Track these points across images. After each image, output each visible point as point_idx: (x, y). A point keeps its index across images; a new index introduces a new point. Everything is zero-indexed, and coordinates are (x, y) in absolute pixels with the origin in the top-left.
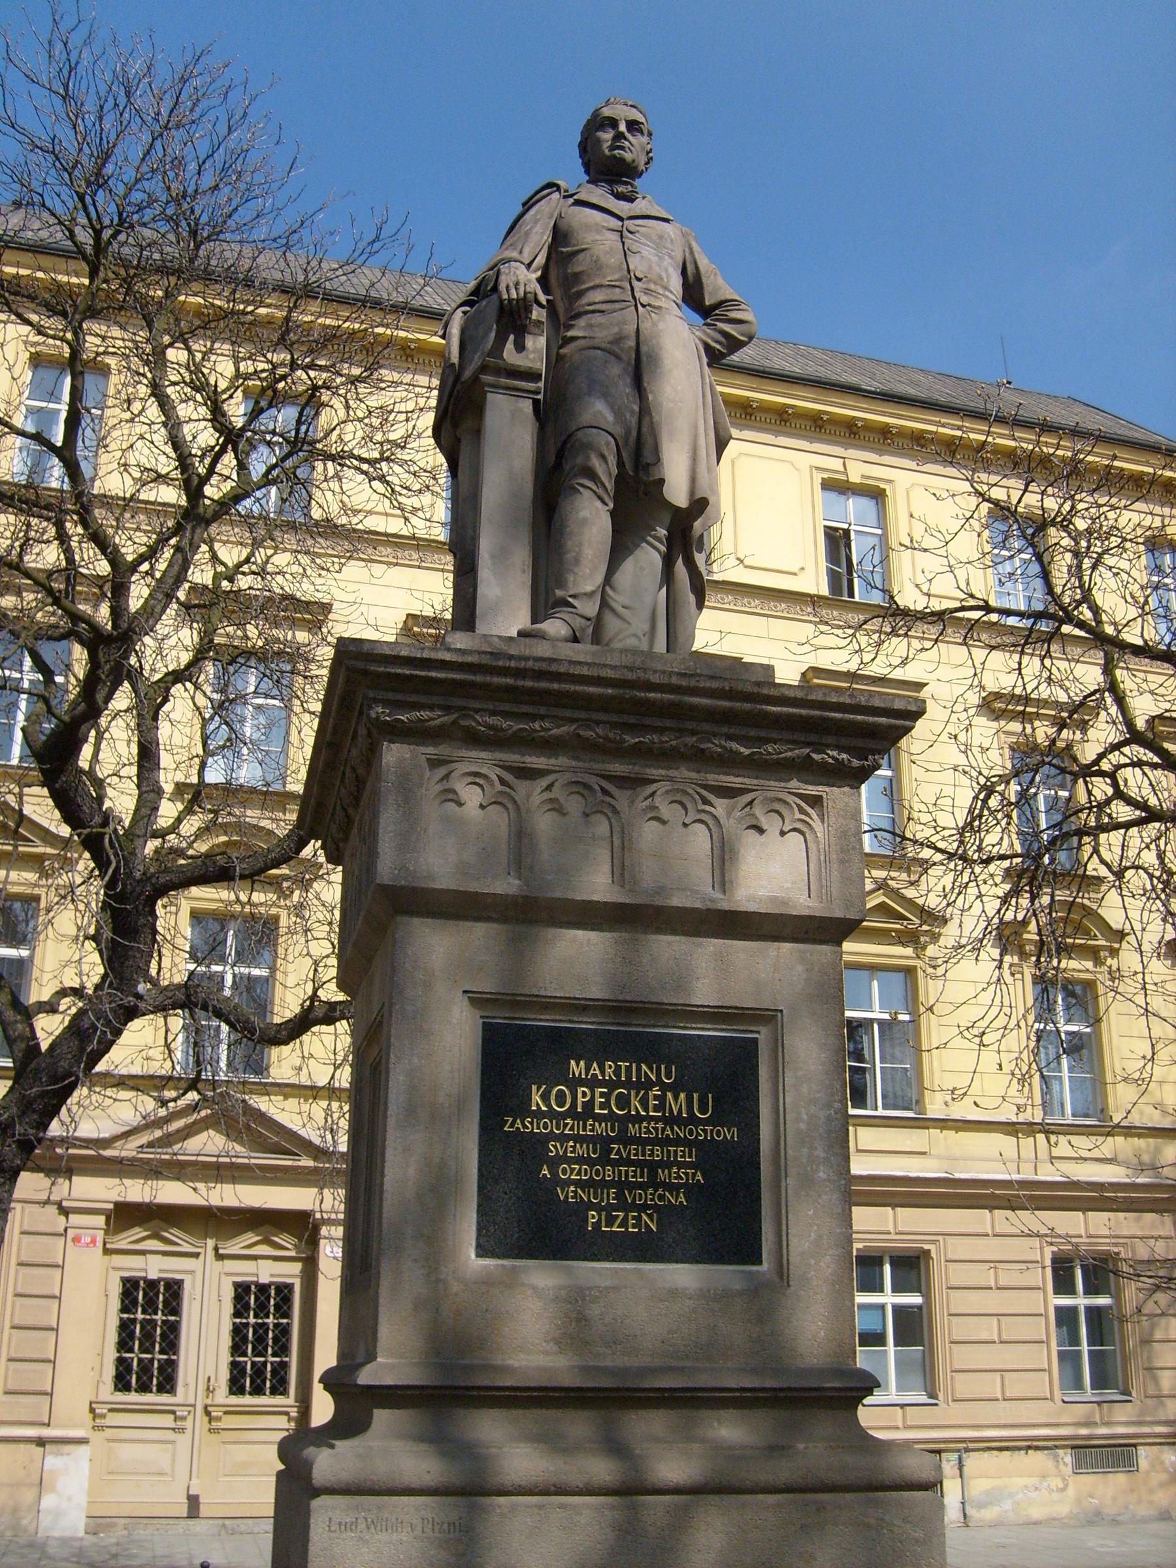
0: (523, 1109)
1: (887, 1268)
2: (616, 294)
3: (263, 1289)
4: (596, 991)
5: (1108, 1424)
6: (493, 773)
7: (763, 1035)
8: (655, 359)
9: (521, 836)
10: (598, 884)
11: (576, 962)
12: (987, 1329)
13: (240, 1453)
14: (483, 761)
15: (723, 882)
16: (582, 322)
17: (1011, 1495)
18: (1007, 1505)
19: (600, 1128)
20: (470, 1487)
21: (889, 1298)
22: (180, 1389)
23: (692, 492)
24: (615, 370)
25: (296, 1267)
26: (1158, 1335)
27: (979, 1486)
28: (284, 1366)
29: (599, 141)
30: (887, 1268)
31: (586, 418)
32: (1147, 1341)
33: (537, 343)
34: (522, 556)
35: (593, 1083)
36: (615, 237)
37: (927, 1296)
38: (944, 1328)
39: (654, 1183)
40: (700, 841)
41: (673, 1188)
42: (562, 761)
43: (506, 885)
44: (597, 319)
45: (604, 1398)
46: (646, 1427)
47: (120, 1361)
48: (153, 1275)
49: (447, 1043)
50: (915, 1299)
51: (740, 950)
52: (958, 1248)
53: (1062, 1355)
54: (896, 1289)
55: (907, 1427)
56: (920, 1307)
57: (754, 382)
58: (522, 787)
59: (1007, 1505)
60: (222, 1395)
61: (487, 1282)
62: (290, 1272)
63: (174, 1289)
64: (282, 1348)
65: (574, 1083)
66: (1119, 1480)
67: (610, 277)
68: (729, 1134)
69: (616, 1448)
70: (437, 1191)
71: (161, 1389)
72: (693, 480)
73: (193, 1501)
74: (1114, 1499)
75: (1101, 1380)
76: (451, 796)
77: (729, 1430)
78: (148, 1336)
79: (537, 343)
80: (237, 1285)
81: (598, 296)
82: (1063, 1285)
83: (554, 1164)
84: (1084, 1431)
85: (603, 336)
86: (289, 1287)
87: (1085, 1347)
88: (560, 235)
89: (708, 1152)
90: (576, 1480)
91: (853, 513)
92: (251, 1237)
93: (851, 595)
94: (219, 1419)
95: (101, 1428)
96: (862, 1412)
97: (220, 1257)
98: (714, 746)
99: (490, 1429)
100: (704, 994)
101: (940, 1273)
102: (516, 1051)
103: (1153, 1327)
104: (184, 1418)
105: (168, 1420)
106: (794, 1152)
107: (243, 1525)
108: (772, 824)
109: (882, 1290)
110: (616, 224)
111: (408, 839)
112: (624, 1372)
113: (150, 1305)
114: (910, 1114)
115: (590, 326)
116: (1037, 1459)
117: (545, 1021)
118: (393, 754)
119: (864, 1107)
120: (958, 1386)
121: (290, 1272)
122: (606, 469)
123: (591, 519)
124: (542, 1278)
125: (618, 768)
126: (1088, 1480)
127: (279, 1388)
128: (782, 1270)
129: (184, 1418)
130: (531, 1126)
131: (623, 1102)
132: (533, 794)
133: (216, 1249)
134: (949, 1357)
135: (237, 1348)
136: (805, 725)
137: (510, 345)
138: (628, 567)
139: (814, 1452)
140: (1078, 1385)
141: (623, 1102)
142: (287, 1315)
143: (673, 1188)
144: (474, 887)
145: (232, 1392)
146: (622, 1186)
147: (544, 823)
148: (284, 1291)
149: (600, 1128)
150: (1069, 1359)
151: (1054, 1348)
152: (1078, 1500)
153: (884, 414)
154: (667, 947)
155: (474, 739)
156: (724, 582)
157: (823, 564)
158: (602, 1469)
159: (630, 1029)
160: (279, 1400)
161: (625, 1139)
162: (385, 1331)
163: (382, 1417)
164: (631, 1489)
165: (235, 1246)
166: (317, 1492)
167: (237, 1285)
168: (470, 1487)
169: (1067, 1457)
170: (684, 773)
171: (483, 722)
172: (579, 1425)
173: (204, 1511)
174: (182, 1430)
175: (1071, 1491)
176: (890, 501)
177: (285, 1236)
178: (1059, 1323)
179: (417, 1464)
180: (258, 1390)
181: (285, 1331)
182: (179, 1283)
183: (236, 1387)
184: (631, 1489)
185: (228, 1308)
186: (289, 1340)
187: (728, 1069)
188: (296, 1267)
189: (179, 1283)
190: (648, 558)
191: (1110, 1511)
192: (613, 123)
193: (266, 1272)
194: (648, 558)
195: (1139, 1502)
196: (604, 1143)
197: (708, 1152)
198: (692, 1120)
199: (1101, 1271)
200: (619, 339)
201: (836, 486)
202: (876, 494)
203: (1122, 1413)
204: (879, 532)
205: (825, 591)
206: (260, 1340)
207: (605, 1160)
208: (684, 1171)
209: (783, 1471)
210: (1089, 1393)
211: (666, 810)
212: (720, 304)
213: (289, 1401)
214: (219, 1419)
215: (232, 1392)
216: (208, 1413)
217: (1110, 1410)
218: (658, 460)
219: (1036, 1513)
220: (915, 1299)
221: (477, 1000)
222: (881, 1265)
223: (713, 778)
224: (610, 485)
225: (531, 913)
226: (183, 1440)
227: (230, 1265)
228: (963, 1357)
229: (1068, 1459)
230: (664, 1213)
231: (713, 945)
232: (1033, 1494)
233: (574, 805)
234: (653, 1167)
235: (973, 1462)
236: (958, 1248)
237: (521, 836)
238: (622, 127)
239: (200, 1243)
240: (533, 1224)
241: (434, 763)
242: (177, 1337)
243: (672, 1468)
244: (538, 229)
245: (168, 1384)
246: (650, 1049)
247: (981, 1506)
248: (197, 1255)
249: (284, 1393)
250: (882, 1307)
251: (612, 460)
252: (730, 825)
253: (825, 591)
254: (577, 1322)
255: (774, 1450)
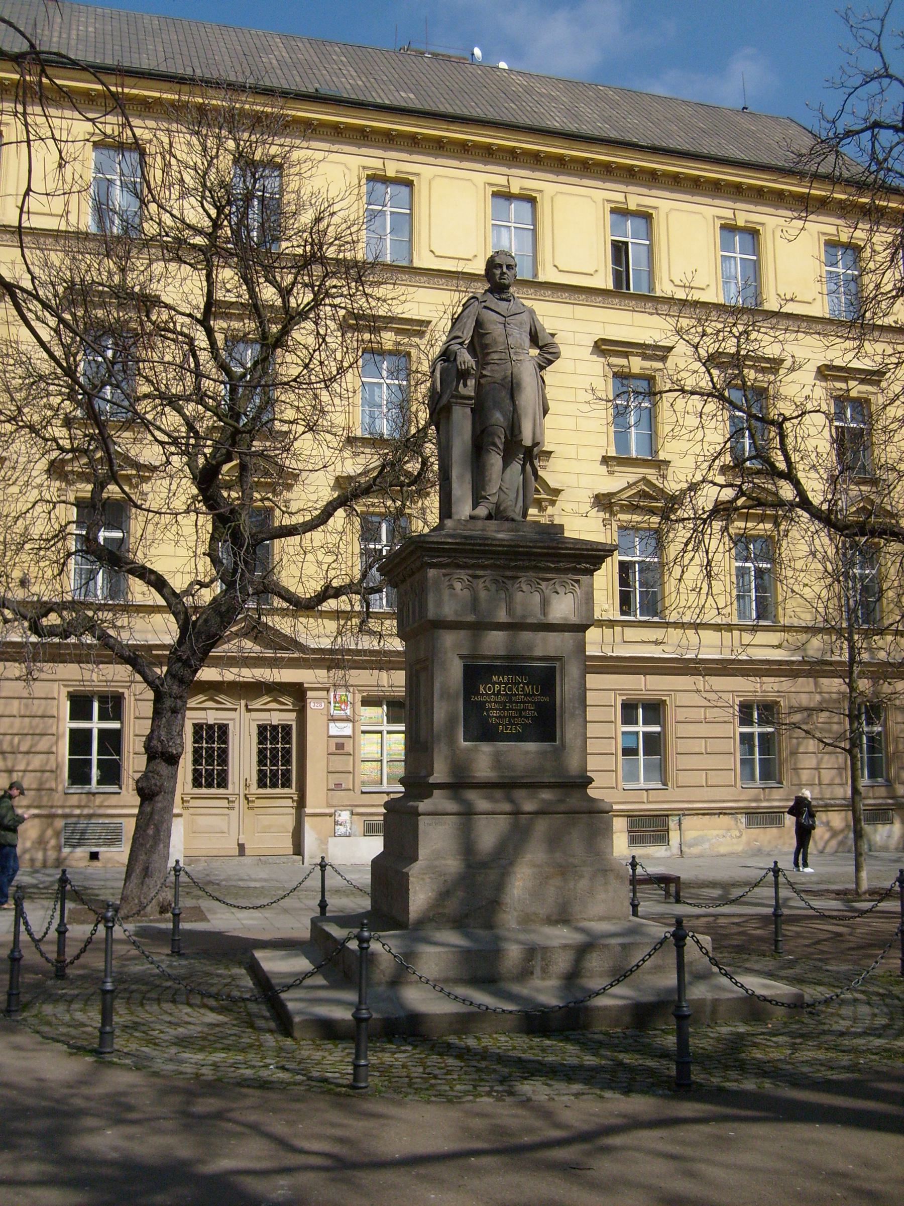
0: (477, 693)
1: (640, 711)
2: (503, 356)
3: (274, 728)
4: (502, 652)
5: (768, 800)
6: (465, 578)
7: (557, 665)
8: (519, 385)
9: (475, 599)
10: (502, 616)
11: (495, 642)
12: (699, 746)
13: (266, 820)
14: (463, 574)
15: (545, 614)
16: (489, 367)
17: (709, 840)
18: (706, 846)
19: (503, 699)
20: (468, 813)
21: (641, 728)
22: (230, 786)
23: (533, 440)
24: (504, 394)
25: (293, 715)
26: (801, 750)
27: (690, 835)
28: (289, 771)
29: (494, 274)
30: (640, 711)
31: (493, 421)
32: (794, 753)
33: (471, 382)
34: (468, 477)
35: (500, 683)
36: (502, 326)
37: (664, 727)
38: (673, 745)
39: (521, 716)
40: (537, 597)
41: (527, 718)
42: (488, 572)
43: (471, 618)
44: (496, 367)
45: (506, 786)
46: (520, 794)
47: (195, 771)
48: (211, 722)
49: (453, 672)
50: (657, 729)
51: (552, 636)
52: (683, 699)
53: (743, 761)
54: (645, 723)
55: (649, 802)
56: (659, 733)
57: (566, 143)
58: (475, 581)
59: (706, 846)
60: (254, 789)
61: (468, 750)
62: (290, 718)
63: (223, 730)
64: (288, 762)
65: (494, 684)
66: (773, 831)
67: (500, 348)
68: (547, 699)
69: (511, 801)
70: (451, 722)
71: (219, 786)
72: (534, 434)
73: (241, 847)
74: (769, 842)
75: (766, 775)
76: (451, 587)
77: (546, 795)
78: (210, 756)
79: (471, 382)
80: (259, 726)
81: (495, 356)
82: (746, 720)
83: (488, 710)
84: (754, 805)
85: (498, 376)
86: (290, 726)
87: (757, 756)
88: (479, 324)
89: (539, 706)
90: (499, 810)
91: (629, 233)
92: (266, 699)
93: (628, 288)
94: (253, 802)
95: (188, 808)
96: (588, 791)
97: (249, 710)
98: (542, 565)
99: (472, 795)
100: (538, 652)
101: (671, 714)
102: (475, 674)
103: (798, 744)
104: (233, 802)
105: (224, 803)
106: (568, 704)
107: (271, 859)
108: (561, 590)
109: (637, 723)
110: (502, 319)
111: (439, 604)
112: (513, 777)
113: (210, 739)
114: (656, 619)
115: (492, 371)
116: (725, 820)
117: (485, 663)
118: (432, 573)
119: (628, 614)
120: (680, 778)
121: (290, 718)
122: (500, 442)
123: (495, 460)
124: (486, 748)
125: (508, 573)
126: (755, 832)
127: (286, 784)
128: (563, 745)
129: (233, 802)
130: (480, 699)
131: (510, 689)
132: (480, 584)
133: (246, 706)
134: (675, 762)
135: (261, 762)
136: (575, 556)
137: (461, 385)
138: (508, 470)
139: (574, 802)
140: (753, 778)
141: (510, 689)
142: (289, 742)
143: (527, 718)
144: (460, 619)
145: (194, 786)
146: (510, 717)
147: (483, 594)
148: (287, 729)
149: (503, 699)
150: (747, 763)
151: (738, 757)
152: (748, 843)
153: (653, 162)
154: (526, 636)
155: (459, 566)
156: (545, 283)
157: (610, 265)
158: (507, 807)
159: (513, 665)
160: (286, 790)
161: (511, 702)
162: (436, 766)
163: (436, 792)
164: (516, 813)
165: (257, 704)
166: (420, 815)
167: (259, 726)
168: (468, 813)
169: (743, 819)
170: (530, 574)
171: (462, 561)
172: (498, 794)
173: (247, 852)
174: (233, 808)
175: (744, 838)
176: (655, 222)
177: (286, 697)
178: (742, 742)
179: (451, 806)
180: (274, 785)
181: (288, 752)
182: (226, 726)
183: (262, 784)
184: (516, 813)
185: (255, 740)
186: (291, 756)
187: (545, 678)
188: (293, 715)
189: (226, 726)
190: (516, 467)
191: (767, 849)
192: (501, 266)
193: (276, 718)
194: (516, 467)
195: (784, 844)
196: (503, 703)
197: (539, 706)
198: (534, 695)
199: (768, 710)
200: (505, 378)
201: (620, 212)
202: (646, 217)
203: (777, 794)
204: (647, 242)
205: (611, 286)
206: (274, 757)
207: (504, 709)
208: (532, 712)
209: (562, 807)
210: (758, 783)
211: (525, 587)
212: (545, 345)
213: (292, 791)
214: (253, 802)
215: (259, 787)
216: (247, 799)
217: (770, 793)
218: (520, 432)
219: (723, 850)
220: (657, 729)
221: (462, 657)
222: (637, 709)
223: (541, 575)
224: (501, 447)
225: (479, 627)
226: (234, 814)
227: (255, 715)
228: (684, 762)
229: (743, 820)
230: (524, 726)
231: (542, 634)
232: (721, 840)
233: (493, 588)
234: (520, 711)
235: (687, 821)
236: (683, 699)
237: (475, 599)
238: (505, 270)
239: (237, 702)
240: (483, 731)
241: (445, 575)
242: (227, 756)
243: (529, 806)
244: (470, 321)
245: (223, 782)
246: (521, 671)
247: (690, 846)
248: (235, 710)
249: (290, 786)
250: (637, 733)
251: (503, 437)
252: (547, 592)
253: (611, 286)
254: (497, 762)
255: (561, 801)
